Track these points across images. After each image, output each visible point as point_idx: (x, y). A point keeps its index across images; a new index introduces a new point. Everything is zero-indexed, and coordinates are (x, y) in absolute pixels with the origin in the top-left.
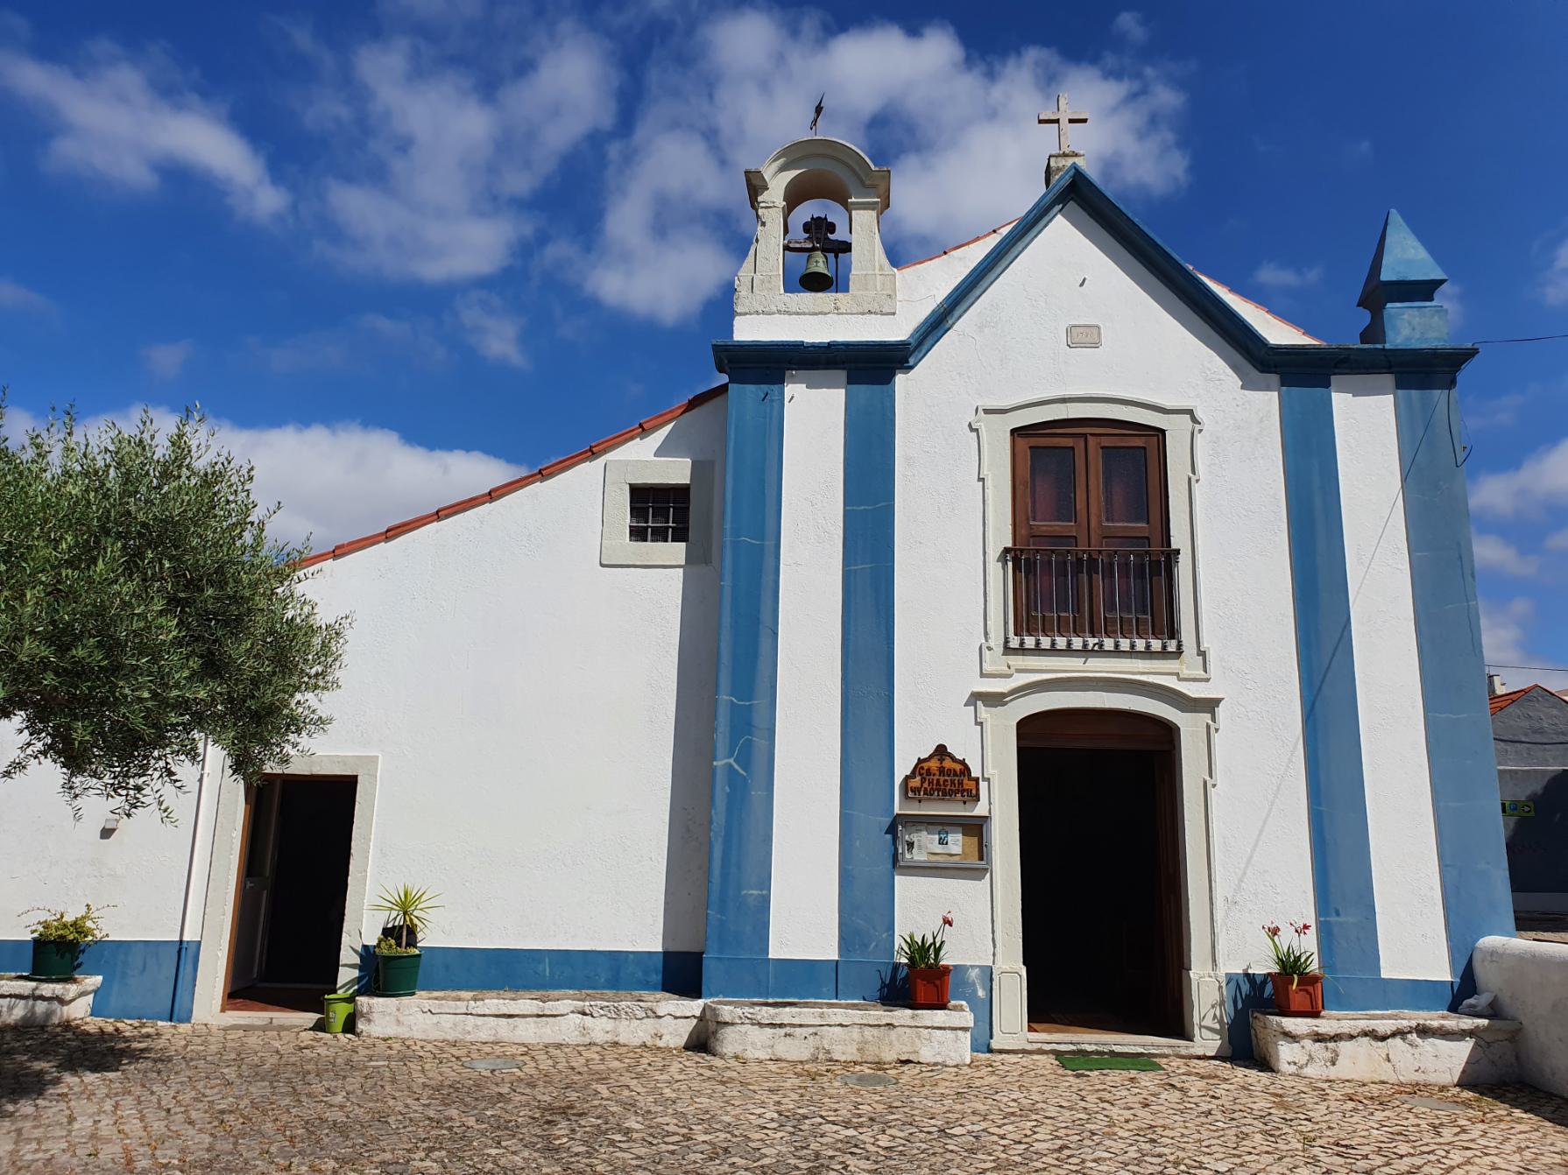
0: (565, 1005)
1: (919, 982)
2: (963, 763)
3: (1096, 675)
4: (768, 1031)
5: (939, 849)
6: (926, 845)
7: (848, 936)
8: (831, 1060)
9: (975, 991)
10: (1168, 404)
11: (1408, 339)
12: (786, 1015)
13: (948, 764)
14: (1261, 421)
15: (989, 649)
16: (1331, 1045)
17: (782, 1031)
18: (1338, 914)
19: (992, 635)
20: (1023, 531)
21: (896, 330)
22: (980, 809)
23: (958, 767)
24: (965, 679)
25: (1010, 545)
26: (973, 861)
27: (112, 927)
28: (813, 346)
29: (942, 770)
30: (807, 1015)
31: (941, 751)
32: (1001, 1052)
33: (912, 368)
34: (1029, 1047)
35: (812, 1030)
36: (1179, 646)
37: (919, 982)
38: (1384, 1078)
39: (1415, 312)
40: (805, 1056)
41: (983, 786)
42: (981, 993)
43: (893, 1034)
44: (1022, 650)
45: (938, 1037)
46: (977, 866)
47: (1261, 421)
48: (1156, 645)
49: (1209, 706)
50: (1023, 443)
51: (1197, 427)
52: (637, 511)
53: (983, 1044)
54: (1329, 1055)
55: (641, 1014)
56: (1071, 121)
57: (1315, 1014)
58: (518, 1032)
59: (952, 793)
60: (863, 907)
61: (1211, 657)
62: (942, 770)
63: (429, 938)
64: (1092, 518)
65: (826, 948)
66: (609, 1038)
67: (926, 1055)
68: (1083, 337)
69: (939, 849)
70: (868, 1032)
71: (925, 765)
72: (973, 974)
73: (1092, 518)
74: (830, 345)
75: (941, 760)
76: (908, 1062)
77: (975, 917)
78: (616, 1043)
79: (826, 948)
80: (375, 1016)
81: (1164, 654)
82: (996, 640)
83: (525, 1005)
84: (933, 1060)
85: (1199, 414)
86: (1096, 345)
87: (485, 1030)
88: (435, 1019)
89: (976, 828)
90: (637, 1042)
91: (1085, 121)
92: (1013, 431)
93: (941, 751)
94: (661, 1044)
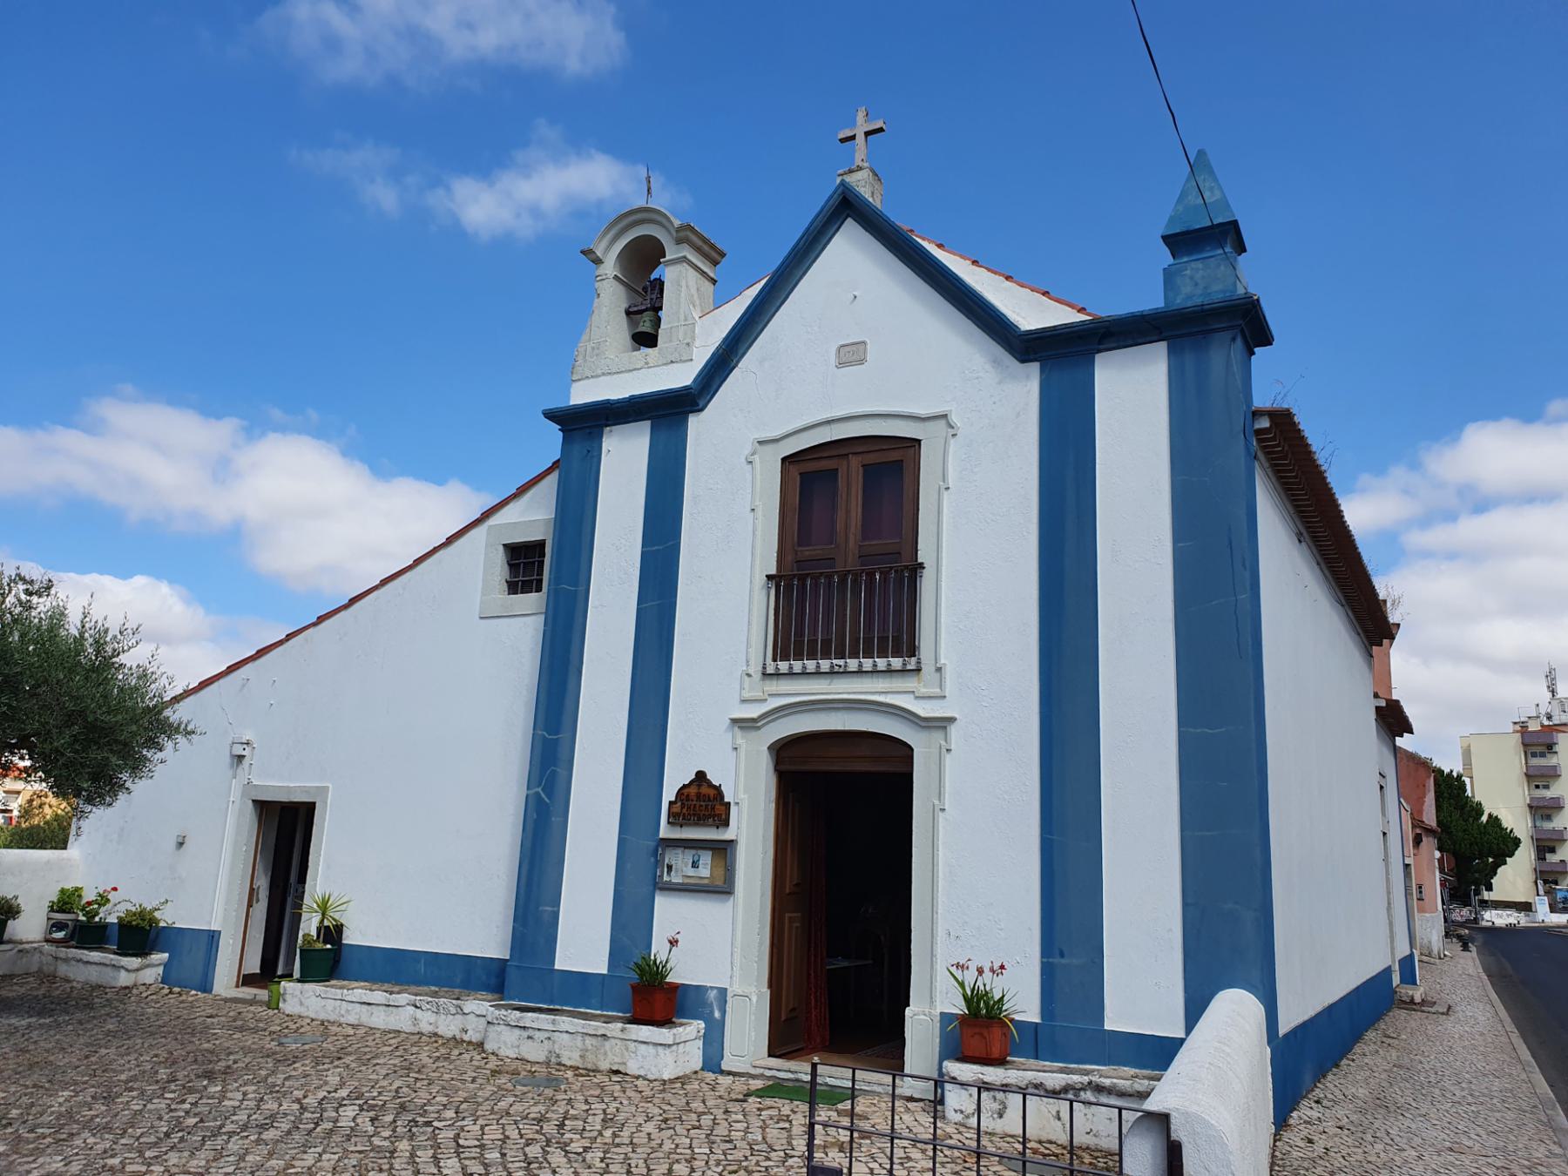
0: (403, 998)
1: (653, 997)
2: (718, 789)
3: (848, 696)
4: (517, 1032)
5: (691, 872)
6: (682, 866)
7: (520, 940)
8: (559, 1064)
9: (712, 1012)
10: (922, 411)
11: (1189, 297)
12: (529, 1018)
13: (705, 790)
14: (1018, 415)
15: (749, 675)
16: (1000, 1095)
17: (525, 1034)
18: (1062, 955)
19: (752, 662)
20: (790, 558)
21: (682, 376)
22: (728, 834)
23: (712, 792)
24: (730, 708)
25: (774, 572)
26: (719, 882)
27: (168, 917)
28: (618, 401)
29: (698, 795)
30: (543, 1020)
31: (701, 776)
32: (729, 1073)
33: (701, 410)
34: (753, 1071)
35: (547, 1035)
36: (919, 663)
37: (653, 997)
38: (1053, 1138)
39: (1200, 265)
40: (542, 1058)
41: (733, 809)
42: (717, 1014)
43: (607, 1044)
44: (777, 675)
45: (665, 1053)
46: (722, 888)
47: (1018, 415)
48: (897, 663)
49: (943, 724)
50: (795, 471)
51: (951, 432)
52: (513, 567)
53: (712, 1062)
54: (996, 1106)
55: (453, 1011)
56: (867, 134)
57: (1000, 1062)
58: (374, 1019)
59: (707, 817)
60: (631, 920)
61: (949, 673)
62: (698, 795)
63: (351, 938)
64: (850, 540)
65: (599, 965)
66: (431, 1029)
67: (633, 1068)
68: (852, 354)
69: (691, 872)
70: (589, 1041)
71: (685, 791)
72: (712, 995)
73: (850, 540)
74: (632, 398)
75: (699, 786)
76: (617, 1072)
77: (721, 941)
78: (436, 1034)
79: (599, 965)
80: (288, 997)
81: (903, 671)
82: (756, 670)
83: (378, 996)
84: (637, 1073)
85: (954, 418)
86: (862, 361)
87: (354, 1015)
88: (323, 1002)
89: (724, 851)
90: (449, 1035)
91: (881, 130)
92: (784, 460)
93: (701, 776)
94: (466, 1038)
